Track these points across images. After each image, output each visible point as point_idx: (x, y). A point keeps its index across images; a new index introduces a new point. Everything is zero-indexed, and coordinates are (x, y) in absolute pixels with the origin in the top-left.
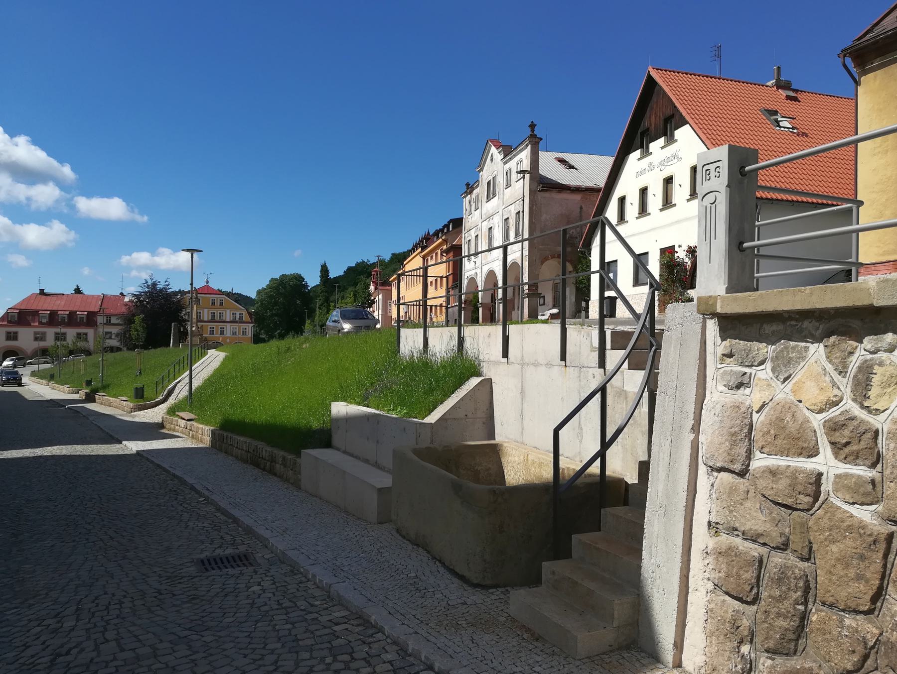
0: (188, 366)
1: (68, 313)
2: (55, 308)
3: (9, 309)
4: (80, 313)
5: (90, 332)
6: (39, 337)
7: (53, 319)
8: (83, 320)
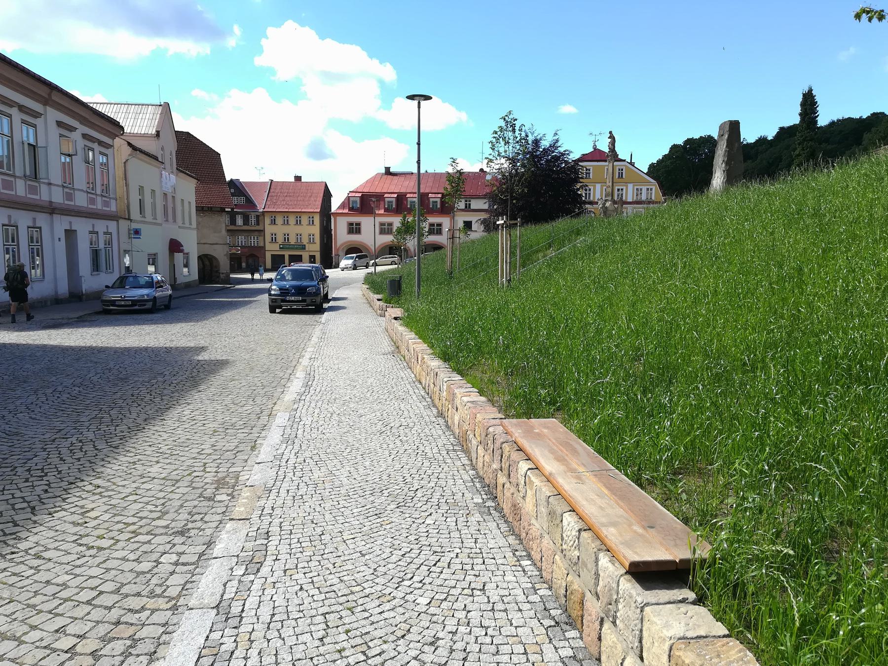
1: (360, 195)
2: (403, 190)
4: (433, 196)
5: (445, 222)
6: (385, 229)
7: (400, 205)
8: (437, 205)
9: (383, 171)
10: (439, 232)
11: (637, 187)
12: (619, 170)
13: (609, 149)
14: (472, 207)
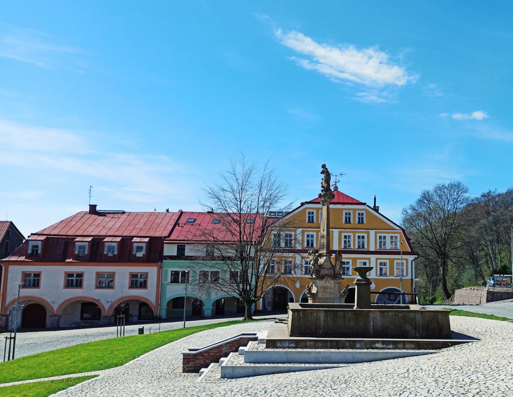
0: (97, 376)
1: (119, 239)
3: (32, 234)
5: (152, 271)
8: (37, 251)
9: (87, 209)
10: (144, 285)
11: (380, 235)
12: (346, 214)
13: (322, 187)
14: (187, 254)
